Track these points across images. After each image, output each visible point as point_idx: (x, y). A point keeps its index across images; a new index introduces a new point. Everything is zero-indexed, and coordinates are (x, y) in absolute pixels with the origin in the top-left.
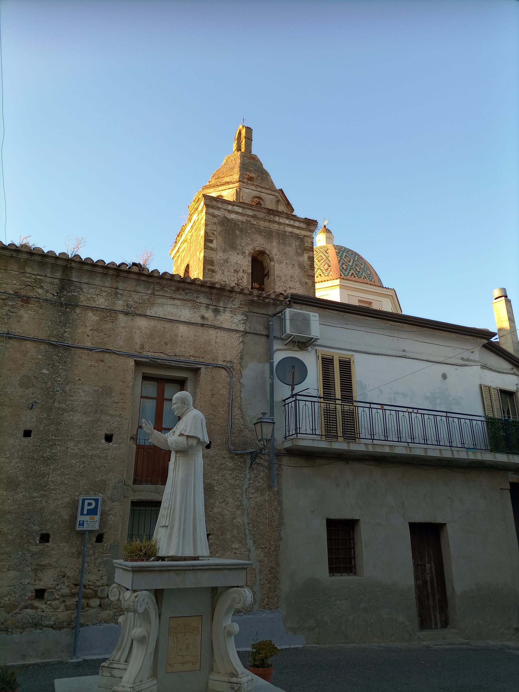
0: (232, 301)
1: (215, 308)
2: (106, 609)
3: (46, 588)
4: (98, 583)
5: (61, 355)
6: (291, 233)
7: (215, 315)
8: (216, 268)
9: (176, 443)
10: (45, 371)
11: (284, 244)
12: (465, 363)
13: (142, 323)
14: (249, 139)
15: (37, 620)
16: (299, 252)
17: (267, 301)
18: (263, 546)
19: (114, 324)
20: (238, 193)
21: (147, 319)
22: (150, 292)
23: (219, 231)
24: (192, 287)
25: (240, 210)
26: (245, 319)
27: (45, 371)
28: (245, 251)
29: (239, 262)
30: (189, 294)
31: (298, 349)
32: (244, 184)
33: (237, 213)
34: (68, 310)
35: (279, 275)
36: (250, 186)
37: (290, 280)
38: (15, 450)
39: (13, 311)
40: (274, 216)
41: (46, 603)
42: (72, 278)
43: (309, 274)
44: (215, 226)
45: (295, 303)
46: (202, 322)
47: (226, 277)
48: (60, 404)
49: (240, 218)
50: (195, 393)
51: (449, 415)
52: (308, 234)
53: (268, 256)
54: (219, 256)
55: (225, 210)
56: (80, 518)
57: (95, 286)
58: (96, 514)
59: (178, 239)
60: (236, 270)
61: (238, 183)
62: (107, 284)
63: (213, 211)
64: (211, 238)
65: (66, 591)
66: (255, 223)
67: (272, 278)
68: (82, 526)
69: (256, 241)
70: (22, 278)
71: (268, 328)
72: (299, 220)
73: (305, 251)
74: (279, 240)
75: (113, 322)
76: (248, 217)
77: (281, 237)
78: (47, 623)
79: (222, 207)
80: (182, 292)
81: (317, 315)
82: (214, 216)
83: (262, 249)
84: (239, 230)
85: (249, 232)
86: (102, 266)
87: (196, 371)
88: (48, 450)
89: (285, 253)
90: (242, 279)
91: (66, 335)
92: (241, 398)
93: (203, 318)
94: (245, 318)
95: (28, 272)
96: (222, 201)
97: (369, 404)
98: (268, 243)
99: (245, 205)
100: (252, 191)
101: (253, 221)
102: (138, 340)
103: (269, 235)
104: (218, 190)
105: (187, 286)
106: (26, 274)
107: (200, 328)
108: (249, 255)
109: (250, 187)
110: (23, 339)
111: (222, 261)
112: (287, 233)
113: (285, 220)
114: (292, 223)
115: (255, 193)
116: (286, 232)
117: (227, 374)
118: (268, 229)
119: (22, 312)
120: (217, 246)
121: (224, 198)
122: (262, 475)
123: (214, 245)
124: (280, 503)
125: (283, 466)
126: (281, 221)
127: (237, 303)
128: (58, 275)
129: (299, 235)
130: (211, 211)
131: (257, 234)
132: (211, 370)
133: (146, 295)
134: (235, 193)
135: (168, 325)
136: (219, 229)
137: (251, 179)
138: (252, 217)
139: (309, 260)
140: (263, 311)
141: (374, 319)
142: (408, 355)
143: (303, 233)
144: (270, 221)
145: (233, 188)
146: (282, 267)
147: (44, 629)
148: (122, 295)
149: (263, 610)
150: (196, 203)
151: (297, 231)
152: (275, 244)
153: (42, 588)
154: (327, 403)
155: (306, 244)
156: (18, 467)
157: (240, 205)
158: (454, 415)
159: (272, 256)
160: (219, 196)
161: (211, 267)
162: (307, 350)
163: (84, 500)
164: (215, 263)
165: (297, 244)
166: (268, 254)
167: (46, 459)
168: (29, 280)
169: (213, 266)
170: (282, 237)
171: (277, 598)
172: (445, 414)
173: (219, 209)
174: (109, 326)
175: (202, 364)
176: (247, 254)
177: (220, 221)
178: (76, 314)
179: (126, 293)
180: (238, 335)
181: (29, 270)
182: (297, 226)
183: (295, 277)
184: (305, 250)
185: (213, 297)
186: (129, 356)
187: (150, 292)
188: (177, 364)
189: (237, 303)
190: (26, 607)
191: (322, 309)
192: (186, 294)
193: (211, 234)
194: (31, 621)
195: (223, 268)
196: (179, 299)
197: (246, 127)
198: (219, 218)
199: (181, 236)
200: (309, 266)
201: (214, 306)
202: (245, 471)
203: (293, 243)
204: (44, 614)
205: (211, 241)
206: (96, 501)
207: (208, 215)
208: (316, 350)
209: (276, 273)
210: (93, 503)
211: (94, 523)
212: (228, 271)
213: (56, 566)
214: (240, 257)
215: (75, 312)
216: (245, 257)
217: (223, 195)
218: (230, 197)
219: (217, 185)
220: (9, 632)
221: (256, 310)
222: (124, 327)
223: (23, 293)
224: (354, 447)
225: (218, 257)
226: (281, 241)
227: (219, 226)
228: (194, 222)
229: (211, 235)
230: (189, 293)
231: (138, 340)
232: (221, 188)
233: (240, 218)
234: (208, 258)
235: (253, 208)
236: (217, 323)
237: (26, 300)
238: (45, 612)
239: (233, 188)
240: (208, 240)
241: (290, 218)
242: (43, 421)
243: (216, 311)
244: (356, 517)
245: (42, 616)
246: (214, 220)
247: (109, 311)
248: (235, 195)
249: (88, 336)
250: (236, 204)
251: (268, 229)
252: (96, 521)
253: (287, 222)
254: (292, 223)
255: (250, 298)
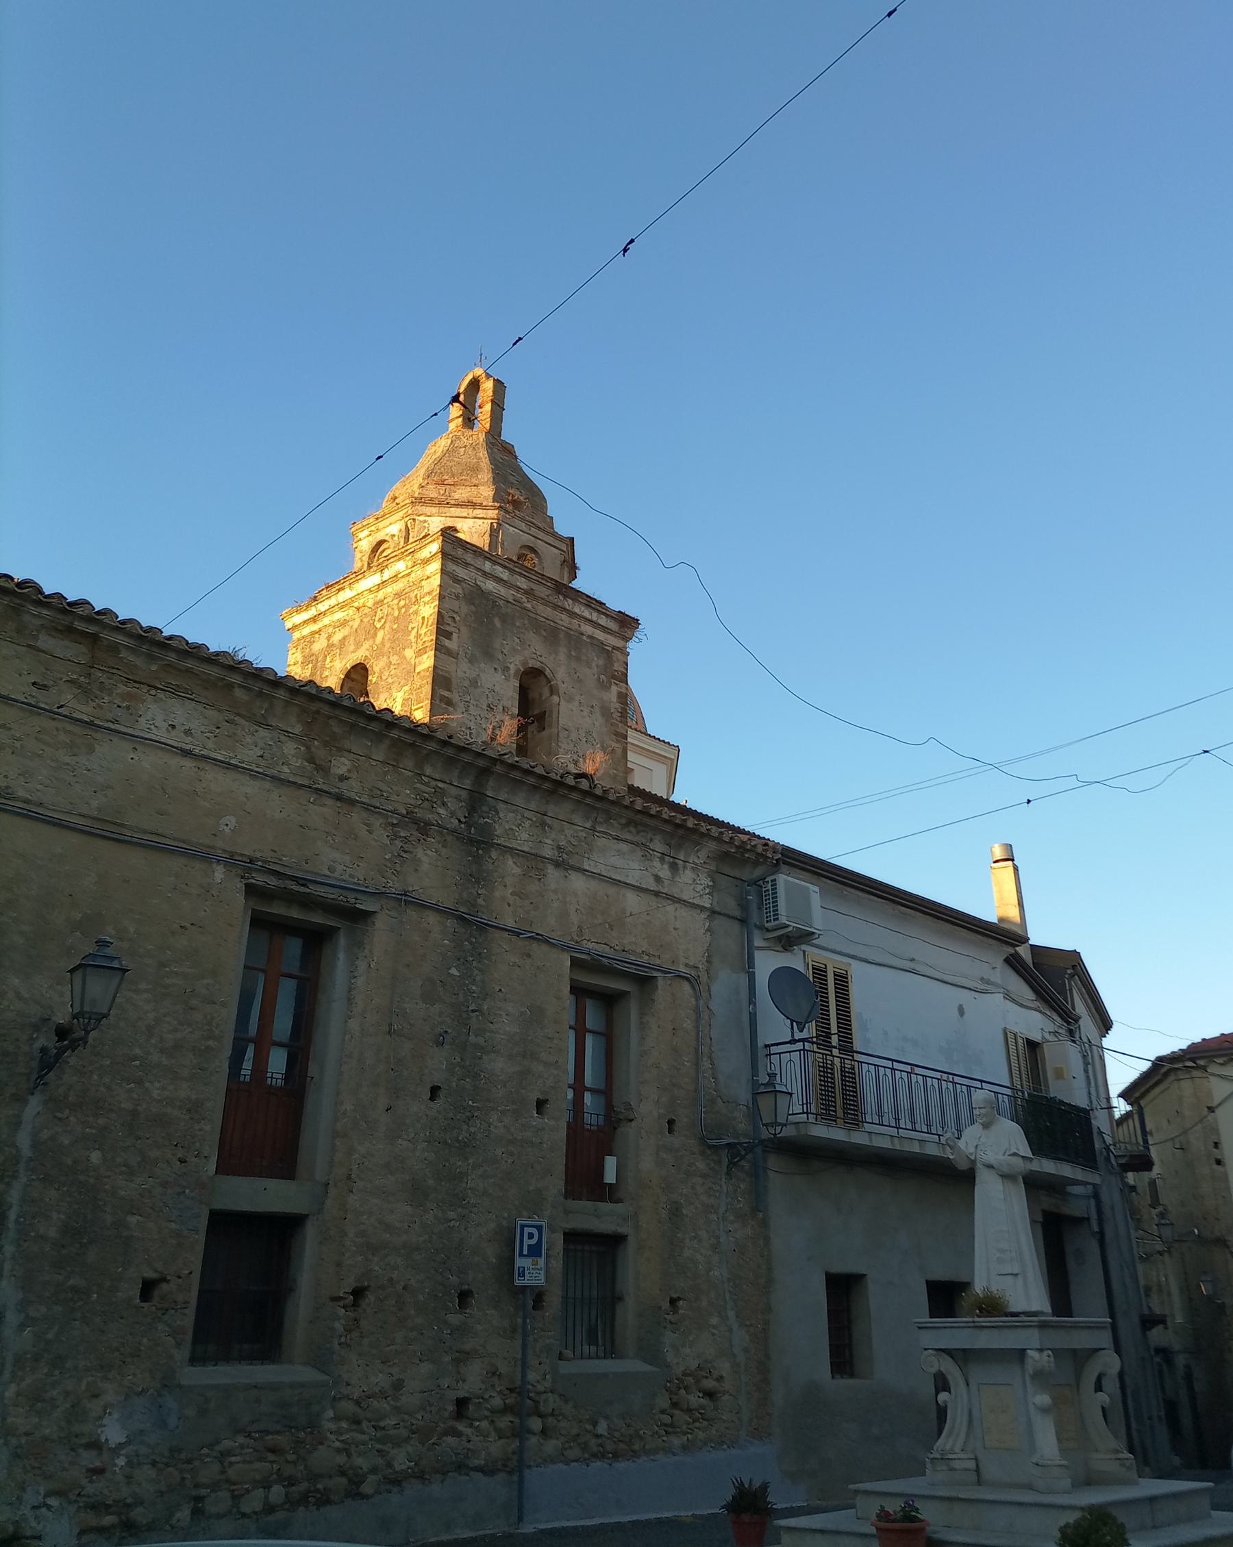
0: (698, 851)
1: (673, 862)
2: (551, 1437)
3: (472, 1396)
4: (540, 1388)
5: (474, 940)
6: (591, 637)
7: (672, 874)
8: (455, 697)
9: (1009, 1165)
10: (454, 971)
11: (578, 659)
12: (984, 988)
13: (578, 883)
14: (499, 406)
15: (462, 1457)
16: (603, 682)
17: (747, 855)
18: (748, 1323)
19: (542, 885)
20: (493, 532)
21: (585, 877)
22: (588, 825)
23: (463, 615)
24: (653, 822)
25: (505, 575)
26: (711, 886)
27: (454, 971)
28: (508, 665)
29: (497, 689)
30: (642, 834)
31: (781, 949)
32: (508, 516)
33: (499, 580)
34: (480, 852)
35: (565, 727)
36: (517, 521)
37: (585, 740)
38: (420, 1126)
39: (406, 849)
40: (564, 599)
41: (471, 1426)
42: (487, 790)
43: (618, 730)
44: (457, 603)
45: (785, 863)
46: (656, 889)
47: (473, 718)
48: (476, 1036)
49: (503, 591)
50: (642, 1023)
51: (896, 1065)
52: (618, 643)
53: (549, 681)
54: (461, 671)
55: (478, 569)
56: (520, 1262)
57: (514, 807)
58: (540, 1256)
59: (324, 592)
60: (491, 706)
61: (497, 511)
62: (533, 806)
63: (455, 567)
64: (448, 628)
65: (497, 1402)
66: (529, 606)
67: (554, 730)
68: (522, 1277)
69: (529, 645)
70: (418, 785)
71: (744, 906)
72: (608, 613)
73: (613, 681)
74: (570, 651)
75: (541, 879)
76: (517, 591)
77: (573, 643)
78: (476, 1462)
79: (472, 563)
80: (632, 829)
81: (817, 889)
82: (457, 580)
83: (538, 665)
84: (499, 618)
85: (518, 624)
86: (540, 774)
87: (644, 981)
88: (465, 1127)
89: (579, 681)
90: (500, 727)
91: (480, 901)
92: (711, 1039)
93: (658, 879)
94: (711, 884)
95: (428, 774)
96: (475, 551)
97: (891, 1062)
98: (550, 654)
99: (516, 567)
100: (521, 533)
101: (526, 600)
102: (575, 919)
103: (552, 635)
104: (448, 515)
105: (646, 820)
106: (423, 778)
107: (653, 898)
108: (515, 674)
109: (517, 522)
110: (423, 906)
111: (466, 683)
112: (584, 638)
113: (583, 608)
114: (594, 616)
115: (526, 539)
116: (583, 634)
117: (691, 992)
118: (552, 623)
119: (420, 853)
120: (459, 647)
121: (460, 535)
122: (742, 1186)
123: (452, 644)
124: (767, 1240)
125: (769, 1171)
126: (576, 611)
127: (703, 854)
128: (468, 783)
129: (606, 645)
130: (451, 567)
131: (531, 632)
132: (670, 982)
133: (582, 831)
134: (489, 532)
135: (612, 890)
136: (465, 609)
137: (516, 504)
138: (526, 592)
139: (619, 700)
140: (736, 873)
141: (880, 900)
142: (920, 968)
143: (613, 641)
144: (556, 607)
145: (483, 518)
146: (572, 711)
147: (472, 1473)
148: (551, 829)
149: (751, 1439)
150: (416, 541)
151: (600, 635)
152: (562, 657)
153: (466, 1395)
154: (823, 1054)
155: (616, 665)
156: (425, 1159)
157: (508, 565)
158: (871, 1060)
159: (555, 682)
160: (450, 528)
161: (446, 694)
162: (791, 951)
163: (522, 1227)
164: (454, 685)
165: (601, 662)
166: (549, 676)
167: (463, 1144)
168: (427, 789)
169: (449, 690)
170: (575, 641)
171: (768, 1416)
172: (889, 1064)
173: (466, 565)
174: (534, 887)
175: (658, 970)
176: (512, 672)
177: (466, 593)
178: (492, 861)
179: (556, 824)
180: (703, 916)
181: (428, 770)
182: (602, 626)
183: (594, 734)
184: (614, 677)
185: (673, 842)
186: (565, 948)
187: (588, 825)
188: (626, 967)
189: (703, 854)
190: (446, 1433)
191: (816, 877)
192: (638, 833)
193: (449, 619)
194: (454, 1458)
195: (468, 699)
196: (626, 841)
197: (494, 379)
198: (464, 585)
199: (339, 590)
200: (619, 715)
201: (671, 857)
202: (721, 1179)
203: (593, 660)
204: (470, 1446)
205: (448, 635)
206: (539, 1228)
207: (446, 577)
208: (804, 952)
209: (561, 722)
210: (535, 1231)
211: (538, 1272)
212: (477, 706)
213: (485, 1354)
214: (500, 677)
215: (490, 857)
216: (507, 679)
217: (458, 528)
218: (476, 536)
219: (448, 503)
220: (426, 1479)
221: (727, 870)
222: (555, 891)
223: (420, 814)
224: (858, 1138)
225: (460, 674)
226: (573, 653)
227: (464, 603)
228: (396, 576)
229: (449, 621)
230: (643, 831)
231: (575, 919)
232: (454, 511)
233: (503, 591)
234: (441, 673)
235: (530, 576)
236: (675, 892)
237: (424, 828)
238: (471, 1443)
239: (483, 518)
240: (442, 632)
241: (593, 606)
242: (456, 1070)
243: (674, 867)
244: (862, 1270)
245: (468, 1449)
246: (455, 588)
247: (534, 859)
248: (487, 536)
249: (509, 905)
250: (500, 561)
251: (552, 623)
252: (541, 1268)
253: (586, 614)
254: (594, 616)
255: (725, 848)
